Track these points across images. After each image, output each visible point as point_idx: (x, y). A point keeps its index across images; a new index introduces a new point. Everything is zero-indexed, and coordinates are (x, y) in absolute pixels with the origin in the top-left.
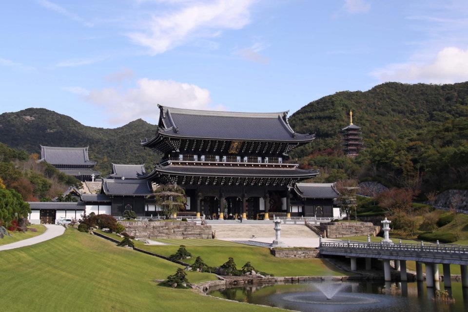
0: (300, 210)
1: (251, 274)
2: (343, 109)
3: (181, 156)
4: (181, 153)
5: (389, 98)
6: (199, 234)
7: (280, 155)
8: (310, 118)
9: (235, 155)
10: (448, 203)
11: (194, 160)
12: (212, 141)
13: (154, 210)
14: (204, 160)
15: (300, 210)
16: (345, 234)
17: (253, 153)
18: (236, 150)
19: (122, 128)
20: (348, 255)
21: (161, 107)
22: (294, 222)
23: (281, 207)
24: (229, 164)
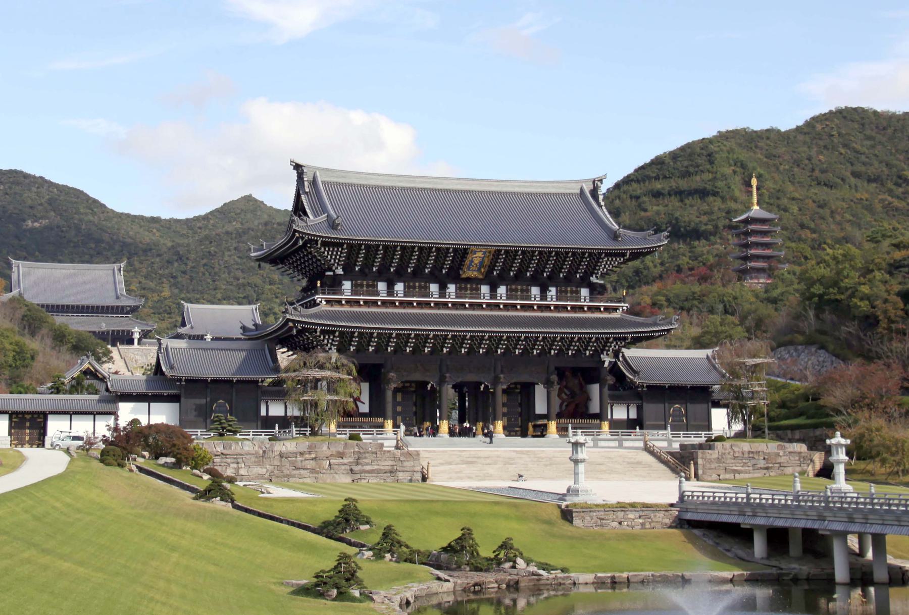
0: (633, 415)
1: (514, 567)
2: (735, 172)
3: (347, 285)
4: (346, 277)
5: (845, 146)
8: (657, 194)
16: (739, 472)
18: (479, 270)
19: (206, 218)
20: (746, 521)
21: (298, 167)
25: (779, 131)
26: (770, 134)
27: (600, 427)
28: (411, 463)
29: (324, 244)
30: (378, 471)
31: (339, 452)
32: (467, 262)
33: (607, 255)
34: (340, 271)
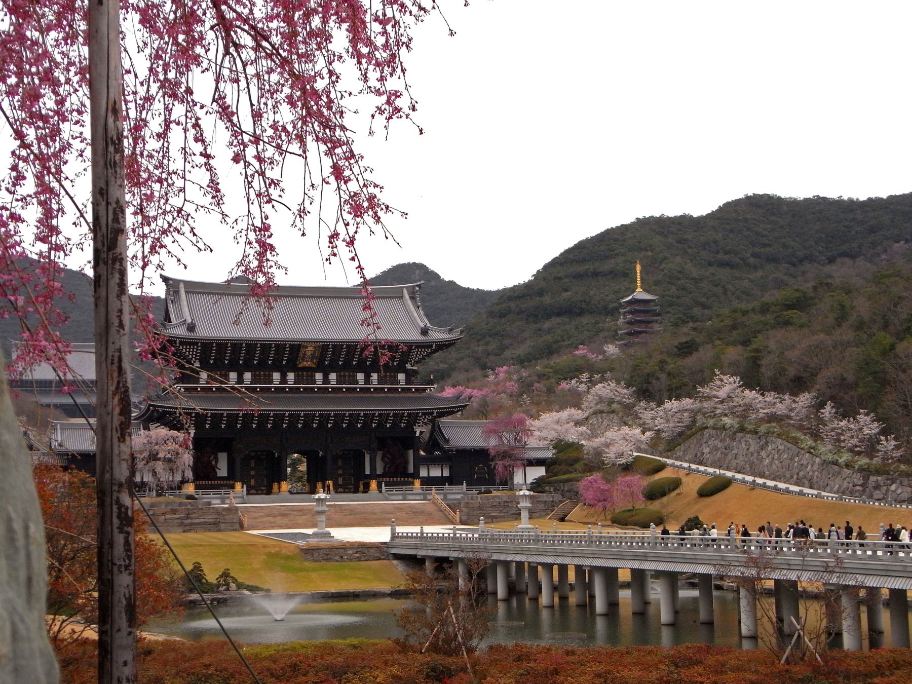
0: (446, 473)
1: (228, 589)
3: (204, 375)
5: (749, 229)
6: (215, 524)
7: (401, 368)
9: (312, 370)
10: (699, 455)
11: (398, 383)
12: (334, 346)
13: (440, 475)
14: (403, 382)
15: (446, 473)
17: (347, 366)
18: (312, 360)
20: (421, 553)
22: (422, 497)
23: (406, 468)
24: (410, 389)
25: (691, 216)
26: (684, 222)
27: (412, 483)
28: (231, 516)
29: (181, 343)
30: (205, 523)
31: (172, 510)
32: (301, 354)
33: (417, 347)
34: (197, 364)
